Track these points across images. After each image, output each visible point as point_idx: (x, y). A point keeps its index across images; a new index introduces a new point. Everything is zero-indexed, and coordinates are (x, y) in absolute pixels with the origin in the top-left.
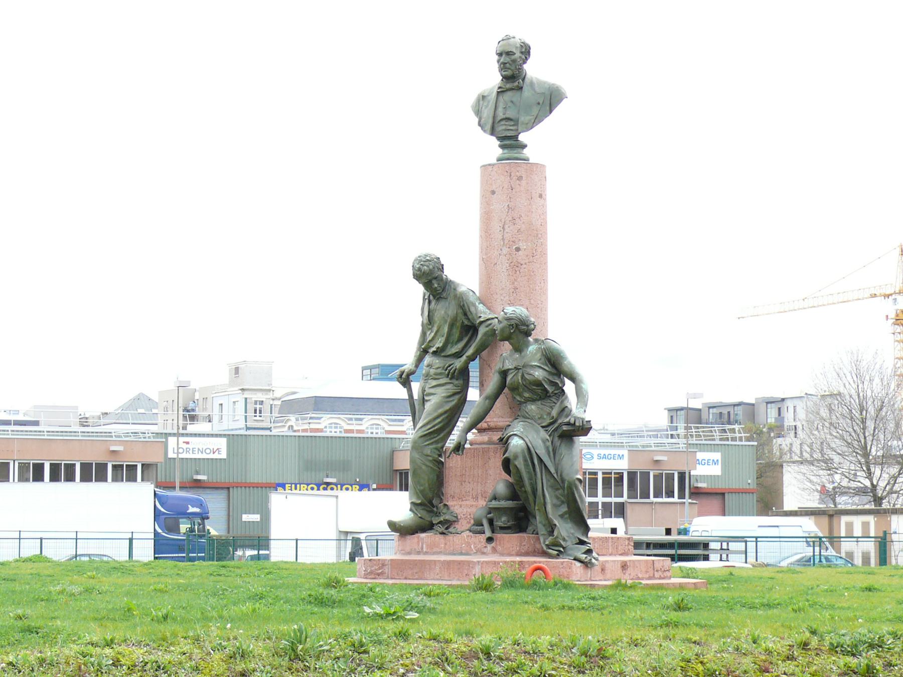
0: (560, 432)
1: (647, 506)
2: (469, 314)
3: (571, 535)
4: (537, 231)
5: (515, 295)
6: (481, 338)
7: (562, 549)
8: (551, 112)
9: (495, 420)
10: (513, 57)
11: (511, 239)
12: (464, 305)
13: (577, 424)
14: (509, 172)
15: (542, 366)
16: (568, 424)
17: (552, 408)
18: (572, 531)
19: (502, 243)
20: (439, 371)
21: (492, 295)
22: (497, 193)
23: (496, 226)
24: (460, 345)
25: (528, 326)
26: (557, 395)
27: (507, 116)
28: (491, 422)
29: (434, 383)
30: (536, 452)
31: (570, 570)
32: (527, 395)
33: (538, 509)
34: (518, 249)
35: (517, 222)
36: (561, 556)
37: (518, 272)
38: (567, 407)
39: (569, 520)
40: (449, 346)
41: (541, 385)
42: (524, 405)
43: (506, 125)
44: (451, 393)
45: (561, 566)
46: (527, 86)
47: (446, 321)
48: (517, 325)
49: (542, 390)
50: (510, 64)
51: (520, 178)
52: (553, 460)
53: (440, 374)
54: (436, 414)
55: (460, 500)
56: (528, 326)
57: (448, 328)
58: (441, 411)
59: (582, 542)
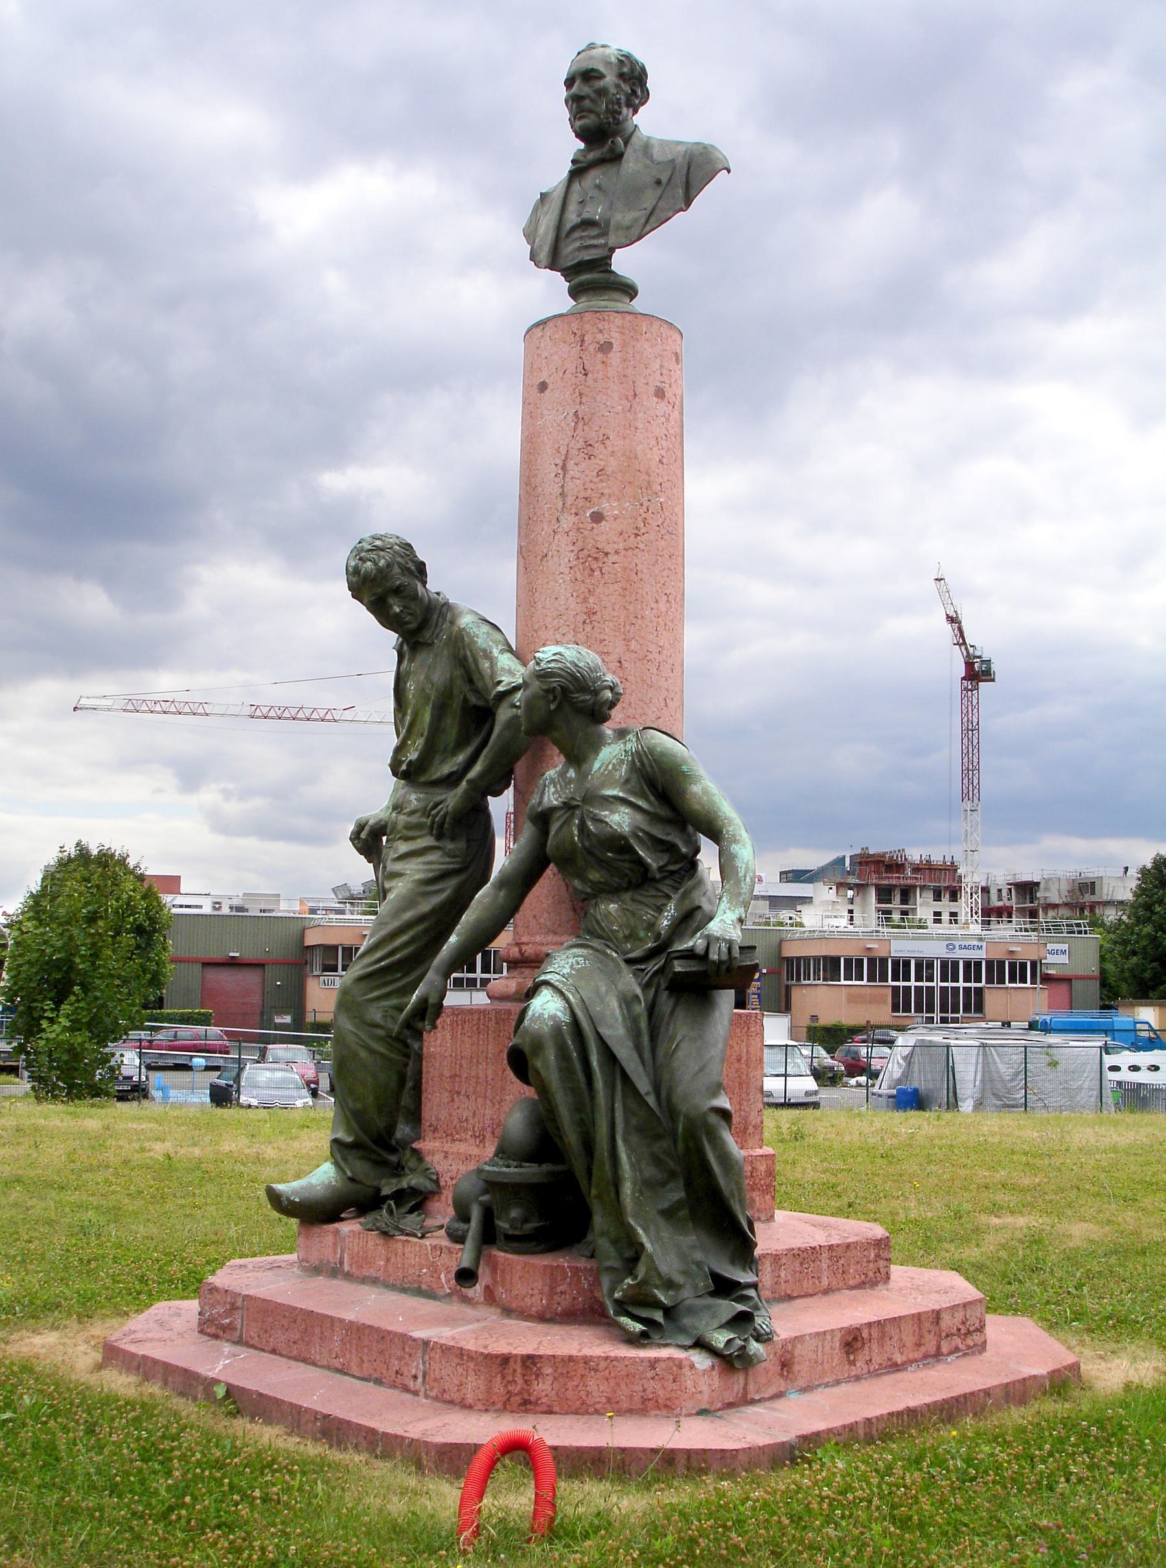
0: (670, 975)
1: (1003, 991)
2: (475, 677)
3: (694, 1267)
4: (647, 474)
5: (588, 628)
6: (499, 735)
7: (658, 1316)
8: (688, 202)
9: (538, 938)
10: (601, 83)
11: (582, 494)
12: (465, 658)
13: (714, 956)
14: (579, 333)
15: (632, 799)
16: (690, 955)
17: (660, 909)
18: (698, 1256)
19: (561, 504)
20: (414, 819)
21: (536, 631)
22: (550, 386)
23: (548, 466)
24: (461, 758)
25: (596, 693)
26: (676, 877)
27: (585, 216)
28: (527, 944)
29: (403, 847)
30: (598, 1033)
31: (675, 1386)
32: (594, 875)
33: (598, 1197)
34: (598, 517)
35: (596, 452)
36: (656, 1337)
37: (597, 573)
38: (699, 907)
39: (691, 1225)
40: (438, 758)
41: (630, 850)
42: (593, 902)
43: (581, 238)
44: (437, 873)
45: (650, 1374)
46: (635, 151)
47: (428, 697)
48: (564, 690)
49: (631, 862)
50: (592, 100)
51: (606, 347)
52: (647, 1055)
53: (419, 826)
54: (396, 924)
55: (449, 1138)
56: (596, 693)
57: (432, 715)
58: (408, 915)
59: (724, 1288)
